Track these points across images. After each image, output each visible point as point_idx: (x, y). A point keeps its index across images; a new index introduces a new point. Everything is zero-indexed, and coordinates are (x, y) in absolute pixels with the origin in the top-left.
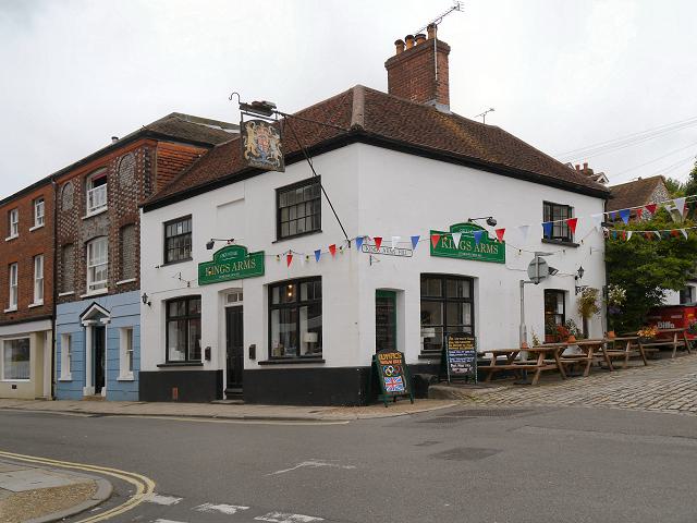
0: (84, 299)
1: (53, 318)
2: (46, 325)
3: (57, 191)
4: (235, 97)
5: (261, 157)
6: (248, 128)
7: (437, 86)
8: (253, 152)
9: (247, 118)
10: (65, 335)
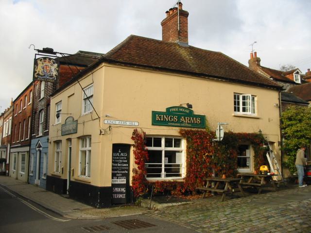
0: (38, 138)
1: (30, 145)
2: (27, 149)
3: (34, 87)
4: (32, 46)
5: (44, 76)
6: (39, 62)
7: (183, 33)
8: (40, 73)
9: (38, 57)
10: (88, 150)
